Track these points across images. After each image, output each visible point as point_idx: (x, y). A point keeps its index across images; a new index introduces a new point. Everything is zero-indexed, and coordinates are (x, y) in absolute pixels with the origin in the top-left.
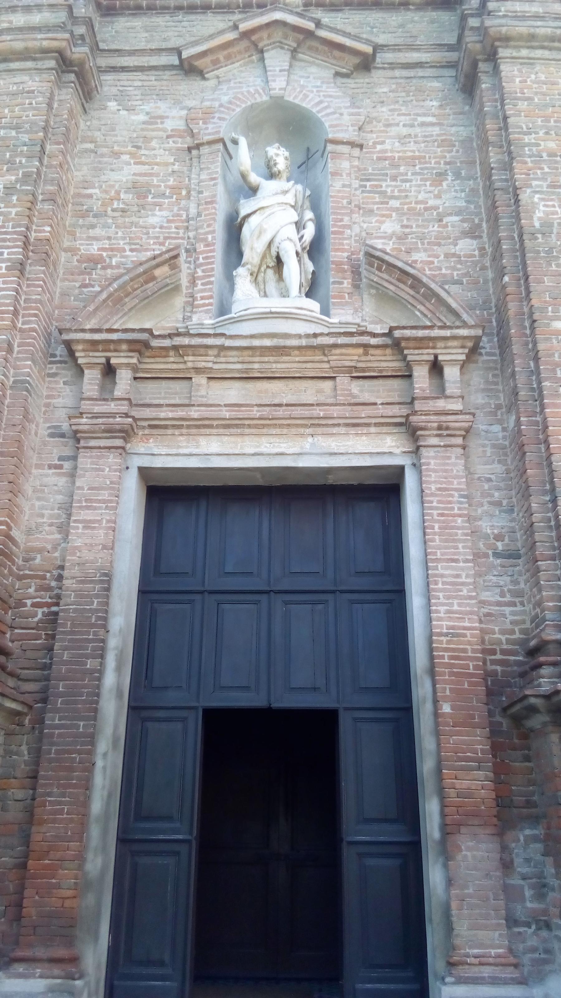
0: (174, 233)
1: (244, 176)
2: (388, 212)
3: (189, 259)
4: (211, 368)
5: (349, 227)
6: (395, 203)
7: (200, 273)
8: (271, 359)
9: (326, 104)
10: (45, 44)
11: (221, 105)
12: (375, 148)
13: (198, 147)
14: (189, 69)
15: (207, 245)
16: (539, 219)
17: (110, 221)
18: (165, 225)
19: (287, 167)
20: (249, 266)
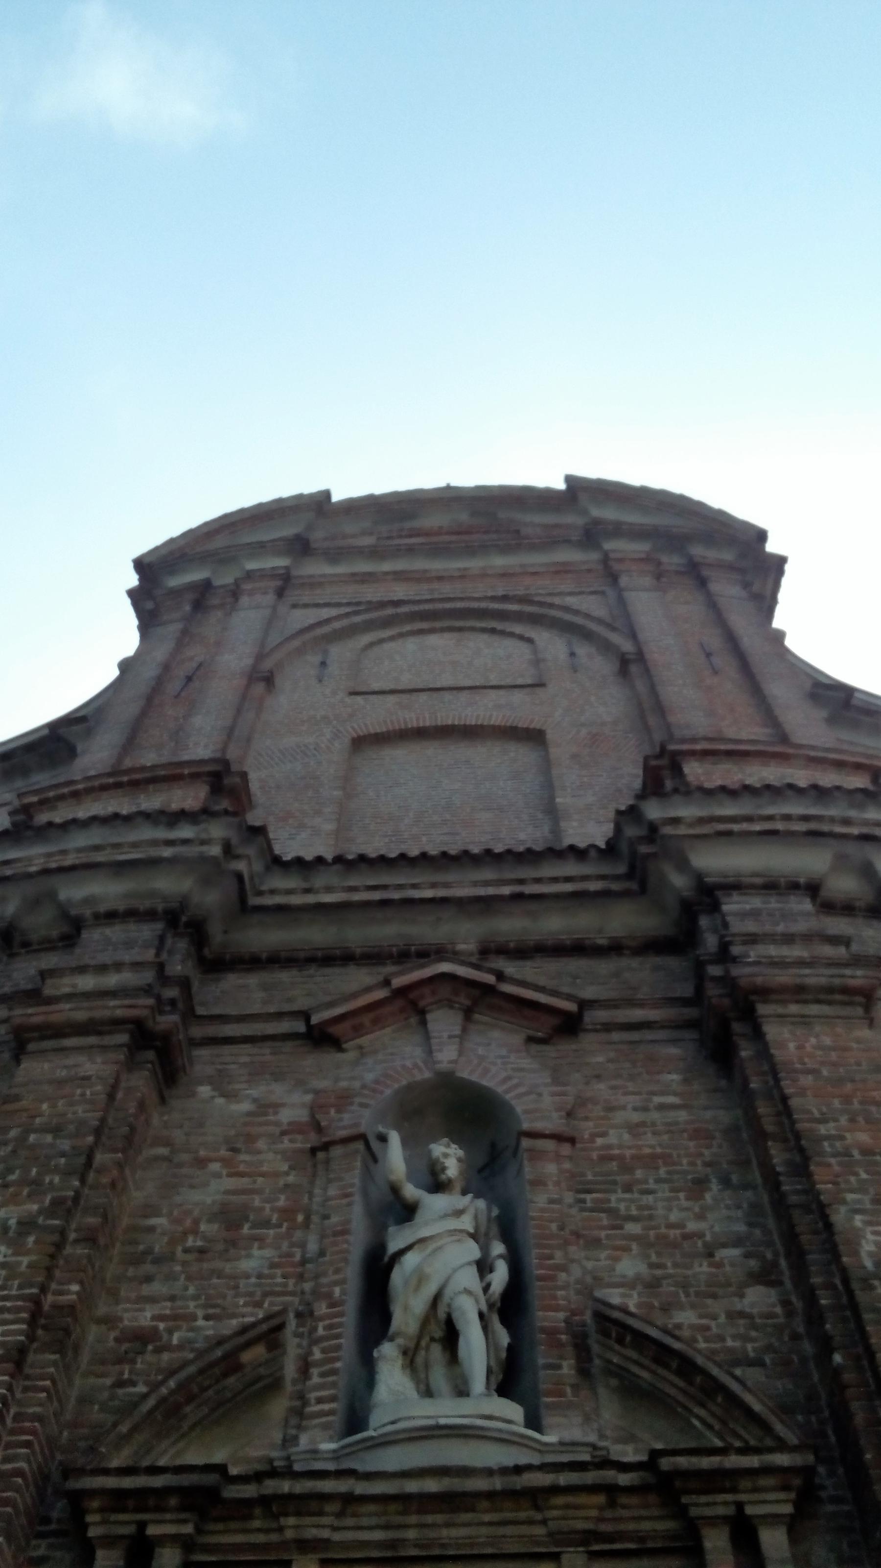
0: (281, 1285)
1: (395, 1190)
2: (624, 1242)
3: (301, 1330)
4: (327, 1541)
5: (563, 1268)
6: (633, 1228)
7: (317, 1355)
8: (439, 1518)
9: (515, 1081)
10: (119, 1013)
11: (364, 1086)
12: (593, 1141)
13: (326, 1147)
14: (321, 1037)
15: (332, 1305)
16: (871, 1254)
17: (178, 1268)
18: (266, 1271)
19: (461, 1173)
20: (400, 1341)
